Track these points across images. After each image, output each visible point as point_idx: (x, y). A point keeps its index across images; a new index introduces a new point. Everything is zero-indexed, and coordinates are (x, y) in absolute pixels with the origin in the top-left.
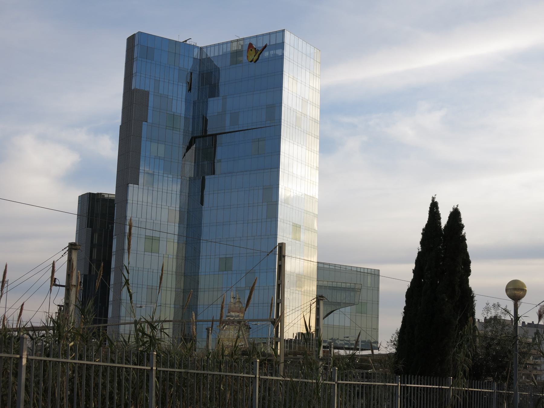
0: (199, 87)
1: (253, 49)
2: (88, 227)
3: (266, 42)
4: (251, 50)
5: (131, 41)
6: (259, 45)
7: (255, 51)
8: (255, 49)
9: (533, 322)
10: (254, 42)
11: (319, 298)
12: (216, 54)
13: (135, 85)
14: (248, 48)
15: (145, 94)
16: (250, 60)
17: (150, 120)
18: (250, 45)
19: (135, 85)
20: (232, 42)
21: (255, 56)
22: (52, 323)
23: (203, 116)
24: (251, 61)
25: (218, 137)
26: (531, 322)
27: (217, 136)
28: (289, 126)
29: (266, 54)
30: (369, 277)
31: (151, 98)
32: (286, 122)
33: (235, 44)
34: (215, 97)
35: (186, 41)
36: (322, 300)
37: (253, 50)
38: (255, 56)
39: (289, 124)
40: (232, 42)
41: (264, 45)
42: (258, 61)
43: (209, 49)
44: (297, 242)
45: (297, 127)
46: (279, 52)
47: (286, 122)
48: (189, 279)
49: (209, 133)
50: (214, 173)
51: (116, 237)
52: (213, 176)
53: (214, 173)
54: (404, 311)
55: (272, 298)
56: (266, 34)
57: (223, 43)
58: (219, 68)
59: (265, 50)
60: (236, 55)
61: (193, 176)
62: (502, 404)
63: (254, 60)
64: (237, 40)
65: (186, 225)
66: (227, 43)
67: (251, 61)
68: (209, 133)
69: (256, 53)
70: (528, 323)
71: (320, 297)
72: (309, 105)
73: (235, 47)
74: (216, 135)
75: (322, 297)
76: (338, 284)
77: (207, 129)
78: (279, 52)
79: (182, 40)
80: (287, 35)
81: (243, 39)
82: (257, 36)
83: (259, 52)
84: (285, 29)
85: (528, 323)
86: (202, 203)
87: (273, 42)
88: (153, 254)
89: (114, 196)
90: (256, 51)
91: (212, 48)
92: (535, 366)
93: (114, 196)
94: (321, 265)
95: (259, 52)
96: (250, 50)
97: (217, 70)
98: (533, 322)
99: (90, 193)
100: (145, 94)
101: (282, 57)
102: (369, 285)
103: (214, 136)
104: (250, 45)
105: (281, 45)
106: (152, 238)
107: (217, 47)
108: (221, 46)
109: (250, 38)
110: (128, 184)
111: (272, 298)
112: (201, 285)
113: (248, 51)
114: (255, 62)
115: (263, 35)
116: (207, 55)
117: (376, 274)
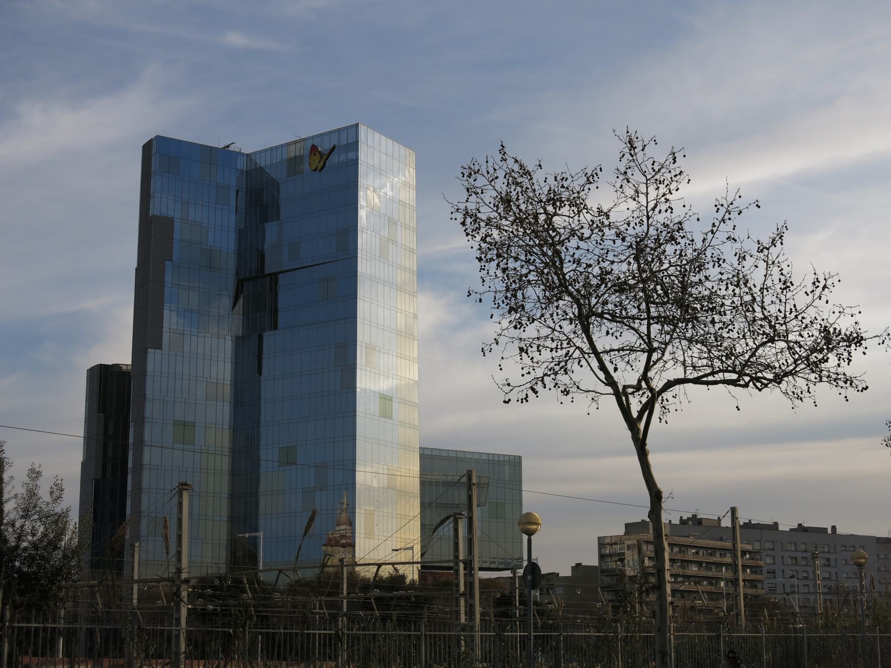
0: (246, 209)
2: (99, 412)
3: (334, 142)
4: (315, 154)
5: (147, 148)
6: (324, 147)
7: (319, 156)
8: (320, 152)
9: (750, 521)
10: (317, 143)
11: (181, 487)
12: (268, 163)
13: (155, 209)
14: (311, 152)
15: (168, 222)
17: (176, 255)
18: (314, 148)
19: (155, 209)
20: (289, 145)
21: (319, 162)
23: (258, 250)
24: (315, 170)
25: (280, 276)
26: (747, 521)
28: (369, 259)
29: (334, 159)
30: (507, 468)
31: (177, 225)
32: (364, 253)
33: (292, 148)
34: (268, 222)
35: (228, 146)
36: (187, 490)
37: (318, 155)
38: (319, 162)
39: (369, 255)
40: (288, 144)
41: (331, 147)
42: (325, 169)
43: (258, 156)
44: (388, 420)
45: (382, 259)
46: (351, 155)
47: (364, 253)
49: (266, 272)
51: (133, 424)
52: (273, 332)
54: (698, 517)
57: (277, 147)
58: (279, 183)
59: (333, 153)
60: (294, 163)
61: (241, 334)
62: (246, 666)
63: (319, 169)
64: (296, 142)
66: (282, 146)
67: (315, 170)
68: (266, 272)
69: (321, 158)
70: (744, 523)
71: (182, 485)
72: (399, 228)
73: (292, 153)
74: (276, 274)
75: (186, 485)
76: (449, 477)
78: (351, 155)
79: (221, 147)
80: (362, 129)
81: (304, 140)
82: (321, 135)
83: (325, 157)
84: (357, 125)
85: (744, 523)
86: (260, 372)
87: (343, 142)
89: (130, 368)
90: (321, 155)
91: (269, 153)
92: (754, 583)
93: (130, 368)
94: (427, 452)
95: (325, 157)
97: (275, 184)
98: (750, 521)
99: (101, 365)
100: (168, 222)
101: (355, 162)
102: (507, 478)
103: (274, 276)
104: (314, 148)
105: (354, 146)
106: (184, 424)
107: (269, 153)
108: (275, 151)
109: (313, 137)
110: (147, 348)
112: (262, 488)
113: (310, 155)
115: (330, 133)
116: (256, 163)
117: (515, 463)
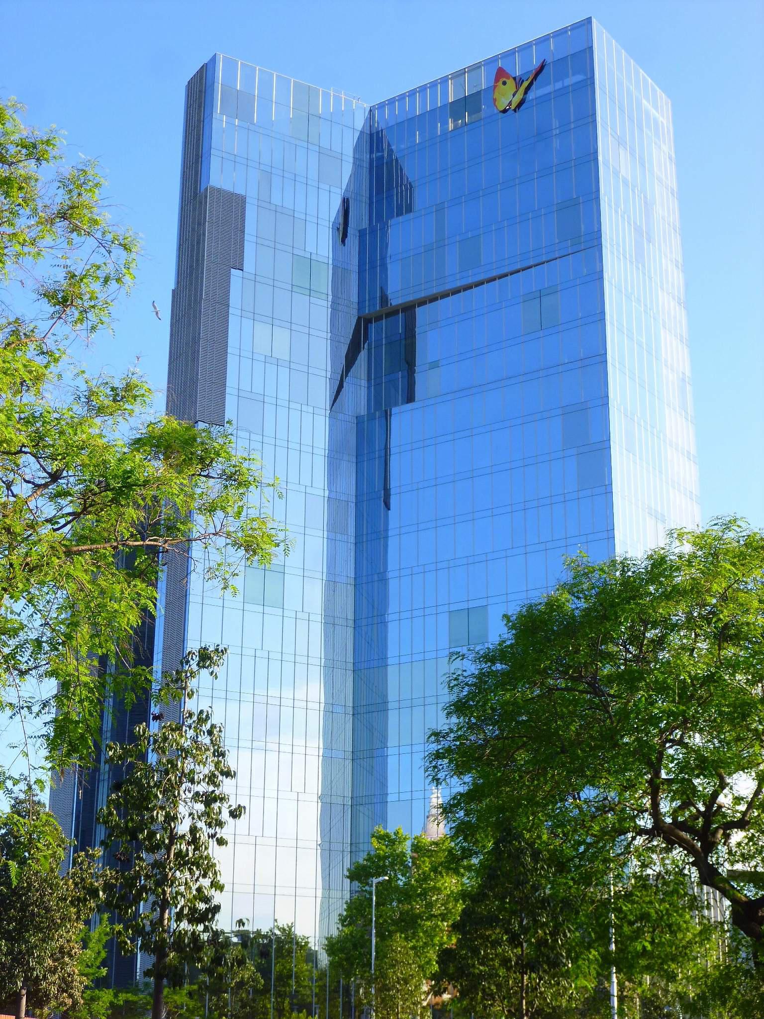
1: (507, 81)
16: (502, 109)
21: (514, 95)
22: (61, 626)
27: (418, 310)
38: (514, 95)
48: (366, 818)
50: (410, 398)
53: (410, 398)
55: (343, 241)
56: (474, 67)
65: (351, 709)
69: (518, 87)
77: (389, 292)
84: (589, 20)
88: (247, 607)
95: (526, 84)
96: (500, 83)
103: (409, 309)
111: (343, 241)
114: (515, 110)
